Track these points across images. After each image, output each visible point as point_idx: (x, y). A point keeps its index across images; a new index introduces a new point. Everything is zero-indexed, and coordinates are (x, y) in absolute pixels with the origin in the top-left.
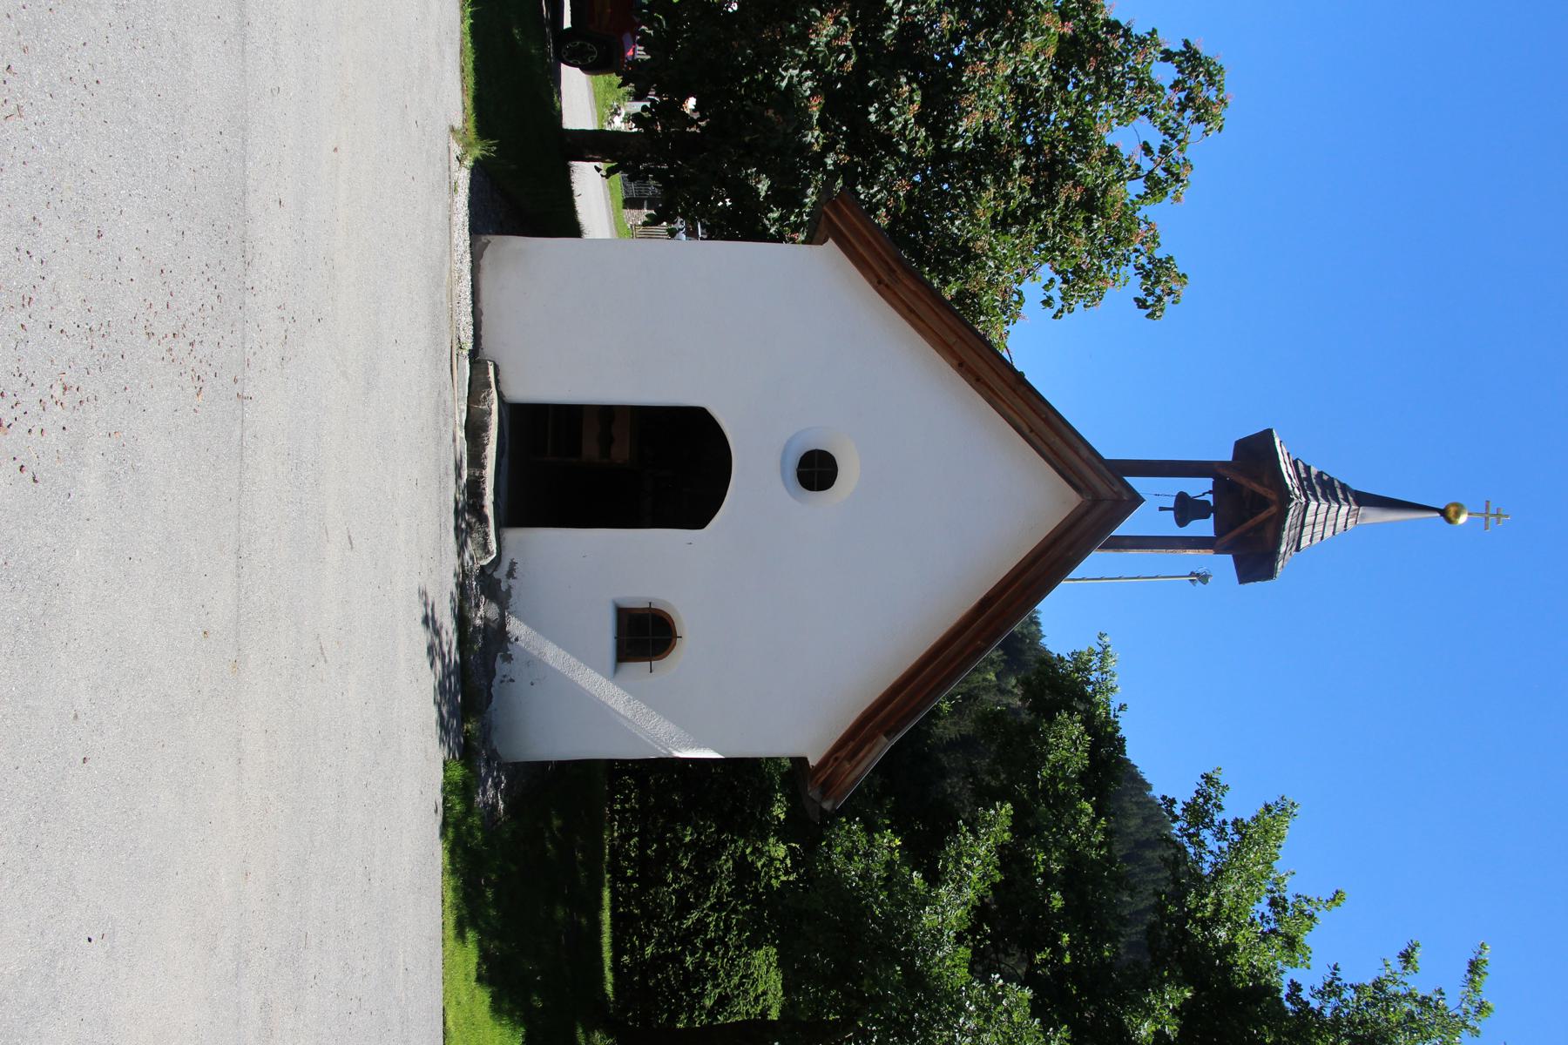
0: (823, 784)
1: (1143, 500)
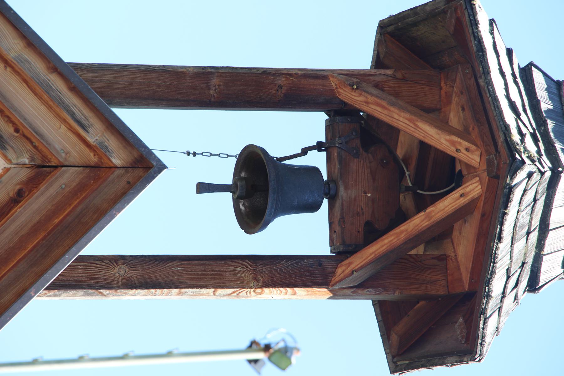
1: (162, 167)
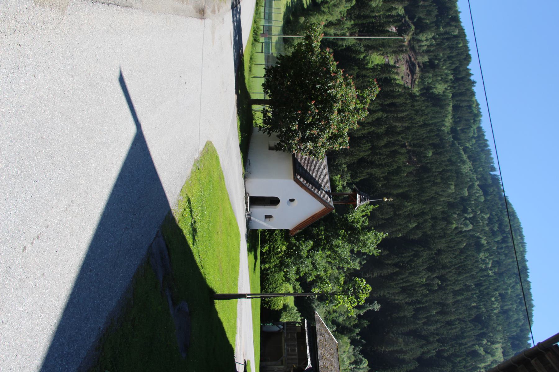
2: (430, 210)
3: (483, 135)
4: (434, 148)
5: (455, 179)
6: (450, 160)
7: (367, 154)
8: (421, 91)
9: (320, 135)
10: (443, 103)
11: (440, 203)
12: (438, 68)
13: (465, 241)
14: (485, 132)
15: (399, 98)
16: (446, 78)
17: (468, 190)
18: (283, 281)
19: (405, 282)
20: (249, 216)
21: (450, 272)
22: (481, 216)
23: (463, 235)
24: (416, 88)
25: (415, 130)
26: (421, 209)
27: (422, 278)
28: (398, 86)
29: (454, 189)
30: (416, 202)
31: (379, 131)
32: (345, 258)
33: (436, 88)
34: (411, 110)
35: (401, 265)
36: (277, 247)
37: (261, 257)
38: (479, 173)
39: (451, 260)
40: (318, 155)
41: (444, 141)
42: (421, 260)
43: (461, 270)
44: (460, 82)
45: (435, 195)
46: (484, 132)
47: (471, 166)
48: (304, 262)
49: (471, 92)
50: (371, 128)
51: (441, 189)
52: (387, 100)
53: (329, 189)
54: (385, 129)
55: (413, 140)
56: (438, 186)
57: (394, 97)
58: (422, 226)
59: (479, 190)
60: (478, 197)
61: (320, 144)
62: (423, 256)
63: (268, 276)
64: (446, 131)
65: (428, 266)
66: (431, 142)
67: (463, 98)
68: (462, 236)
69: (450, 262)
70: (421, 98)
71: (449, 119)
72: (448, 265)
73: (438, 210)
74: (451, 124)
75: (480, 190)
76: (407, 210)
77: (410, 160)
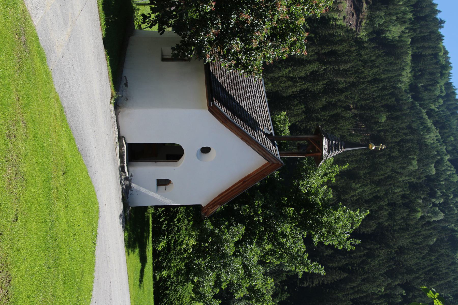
0: (205, 213)
2: (386, 194)
3: (454, 93)
4: (388, 111)
5: (418, 152)
6: (409, 127)
7: (299, 119)
8: (369, 36)
9: (257, 25)
10: (398, 51)
11: (399, 184)
12: (394, 5)
13: (435, 235)
14: (457, 89)
15: (341, 44)
16: (403, 18)
17: (435, 167)
18: (193, 299)
19: (358, 292)
20: (127, 183)
21: (418, 278)
22: (455, 202)
23: (431, 227)
24: (363, 31)
25: (362, 86)
26: (374, 192)
27: (379, 286)
28: (339, 28)
29: (417, 164)
30: (367, 183)
31: (315, 89)
32: (299, 256)
33: (390, 31)
34: (357, 60)
35: (351, 268)
36: (180, 241)
37: (154, 259)
38: (449, 144)
39: (418, 261)
40: (252, 66)
41: (401, 102)
42: (377, 262)
43: (433, 275)
44: (423, 23)
45: (393, 174)
46: (455, 89)
47: (438, 134)
48: (230, 264)
49: (437, 36)
50: (304, 84)
51: (400, 165)
52: (325, 47)
53: (270, 130)
54: (324, 86)
55: (359, 100)
56: (395, 161)
57: (335, 43)
58: (376, 215)
59: (450, 167)
60: (450, 176)
61: (255, 44)
62: (379, 255)
63: (167, 290)
64: (404, 89)
65: (387, 269)
66: (384, 103)
67: (426, 44)
68: (431, 228)
69: (416, 264)
70: (370, 44)
71: (407, 73)
72: (415, 268)
73: (396, 193)
74: (410, 79)
75: (452, 166)
76: (354, 194)
77: (356, 128)
